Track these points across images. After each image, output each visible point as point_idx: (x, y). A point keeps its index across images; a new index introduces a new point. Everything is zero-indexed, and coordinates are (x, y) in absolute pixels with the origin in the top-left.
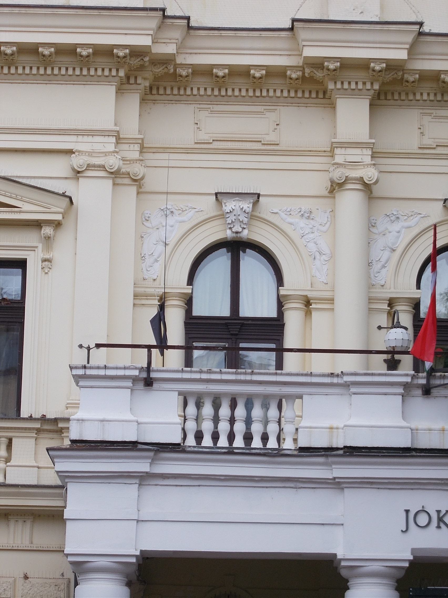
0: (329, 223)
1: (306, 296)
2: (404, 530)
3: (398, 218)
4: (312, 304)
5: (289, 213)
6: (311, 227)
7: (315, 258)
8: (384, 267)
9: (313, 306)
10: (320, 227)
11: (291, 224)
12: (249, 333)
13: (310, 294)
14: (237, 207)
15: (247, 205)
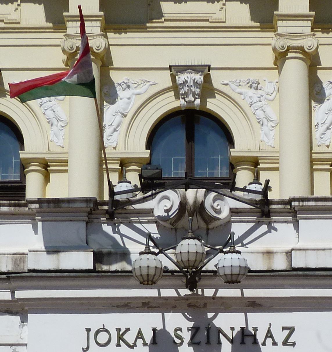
0: (275, 93)
1: (44, 159)
2: (85, 347)
3: (129, 87)
4: (261, 164)
5: (239, 84)
6: (259, 96)
7: (262, 125)
8: (115, 130)
9: (261, 166)
10: (268, 97)
11: (241, 94)
12: (17, 195)
13: (47, 157)
14: (189, 78)
15: (199, 78)
